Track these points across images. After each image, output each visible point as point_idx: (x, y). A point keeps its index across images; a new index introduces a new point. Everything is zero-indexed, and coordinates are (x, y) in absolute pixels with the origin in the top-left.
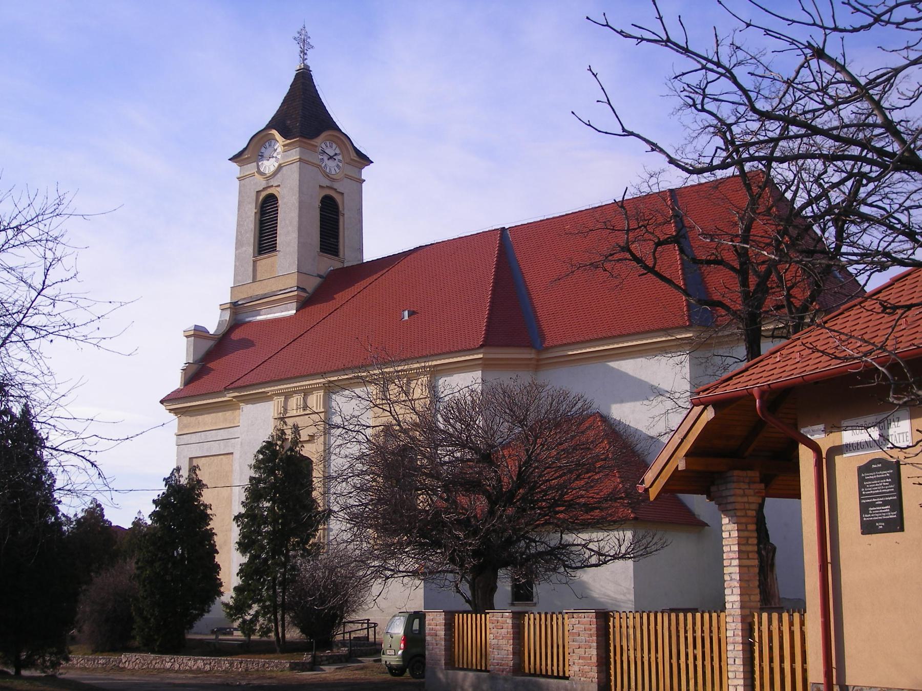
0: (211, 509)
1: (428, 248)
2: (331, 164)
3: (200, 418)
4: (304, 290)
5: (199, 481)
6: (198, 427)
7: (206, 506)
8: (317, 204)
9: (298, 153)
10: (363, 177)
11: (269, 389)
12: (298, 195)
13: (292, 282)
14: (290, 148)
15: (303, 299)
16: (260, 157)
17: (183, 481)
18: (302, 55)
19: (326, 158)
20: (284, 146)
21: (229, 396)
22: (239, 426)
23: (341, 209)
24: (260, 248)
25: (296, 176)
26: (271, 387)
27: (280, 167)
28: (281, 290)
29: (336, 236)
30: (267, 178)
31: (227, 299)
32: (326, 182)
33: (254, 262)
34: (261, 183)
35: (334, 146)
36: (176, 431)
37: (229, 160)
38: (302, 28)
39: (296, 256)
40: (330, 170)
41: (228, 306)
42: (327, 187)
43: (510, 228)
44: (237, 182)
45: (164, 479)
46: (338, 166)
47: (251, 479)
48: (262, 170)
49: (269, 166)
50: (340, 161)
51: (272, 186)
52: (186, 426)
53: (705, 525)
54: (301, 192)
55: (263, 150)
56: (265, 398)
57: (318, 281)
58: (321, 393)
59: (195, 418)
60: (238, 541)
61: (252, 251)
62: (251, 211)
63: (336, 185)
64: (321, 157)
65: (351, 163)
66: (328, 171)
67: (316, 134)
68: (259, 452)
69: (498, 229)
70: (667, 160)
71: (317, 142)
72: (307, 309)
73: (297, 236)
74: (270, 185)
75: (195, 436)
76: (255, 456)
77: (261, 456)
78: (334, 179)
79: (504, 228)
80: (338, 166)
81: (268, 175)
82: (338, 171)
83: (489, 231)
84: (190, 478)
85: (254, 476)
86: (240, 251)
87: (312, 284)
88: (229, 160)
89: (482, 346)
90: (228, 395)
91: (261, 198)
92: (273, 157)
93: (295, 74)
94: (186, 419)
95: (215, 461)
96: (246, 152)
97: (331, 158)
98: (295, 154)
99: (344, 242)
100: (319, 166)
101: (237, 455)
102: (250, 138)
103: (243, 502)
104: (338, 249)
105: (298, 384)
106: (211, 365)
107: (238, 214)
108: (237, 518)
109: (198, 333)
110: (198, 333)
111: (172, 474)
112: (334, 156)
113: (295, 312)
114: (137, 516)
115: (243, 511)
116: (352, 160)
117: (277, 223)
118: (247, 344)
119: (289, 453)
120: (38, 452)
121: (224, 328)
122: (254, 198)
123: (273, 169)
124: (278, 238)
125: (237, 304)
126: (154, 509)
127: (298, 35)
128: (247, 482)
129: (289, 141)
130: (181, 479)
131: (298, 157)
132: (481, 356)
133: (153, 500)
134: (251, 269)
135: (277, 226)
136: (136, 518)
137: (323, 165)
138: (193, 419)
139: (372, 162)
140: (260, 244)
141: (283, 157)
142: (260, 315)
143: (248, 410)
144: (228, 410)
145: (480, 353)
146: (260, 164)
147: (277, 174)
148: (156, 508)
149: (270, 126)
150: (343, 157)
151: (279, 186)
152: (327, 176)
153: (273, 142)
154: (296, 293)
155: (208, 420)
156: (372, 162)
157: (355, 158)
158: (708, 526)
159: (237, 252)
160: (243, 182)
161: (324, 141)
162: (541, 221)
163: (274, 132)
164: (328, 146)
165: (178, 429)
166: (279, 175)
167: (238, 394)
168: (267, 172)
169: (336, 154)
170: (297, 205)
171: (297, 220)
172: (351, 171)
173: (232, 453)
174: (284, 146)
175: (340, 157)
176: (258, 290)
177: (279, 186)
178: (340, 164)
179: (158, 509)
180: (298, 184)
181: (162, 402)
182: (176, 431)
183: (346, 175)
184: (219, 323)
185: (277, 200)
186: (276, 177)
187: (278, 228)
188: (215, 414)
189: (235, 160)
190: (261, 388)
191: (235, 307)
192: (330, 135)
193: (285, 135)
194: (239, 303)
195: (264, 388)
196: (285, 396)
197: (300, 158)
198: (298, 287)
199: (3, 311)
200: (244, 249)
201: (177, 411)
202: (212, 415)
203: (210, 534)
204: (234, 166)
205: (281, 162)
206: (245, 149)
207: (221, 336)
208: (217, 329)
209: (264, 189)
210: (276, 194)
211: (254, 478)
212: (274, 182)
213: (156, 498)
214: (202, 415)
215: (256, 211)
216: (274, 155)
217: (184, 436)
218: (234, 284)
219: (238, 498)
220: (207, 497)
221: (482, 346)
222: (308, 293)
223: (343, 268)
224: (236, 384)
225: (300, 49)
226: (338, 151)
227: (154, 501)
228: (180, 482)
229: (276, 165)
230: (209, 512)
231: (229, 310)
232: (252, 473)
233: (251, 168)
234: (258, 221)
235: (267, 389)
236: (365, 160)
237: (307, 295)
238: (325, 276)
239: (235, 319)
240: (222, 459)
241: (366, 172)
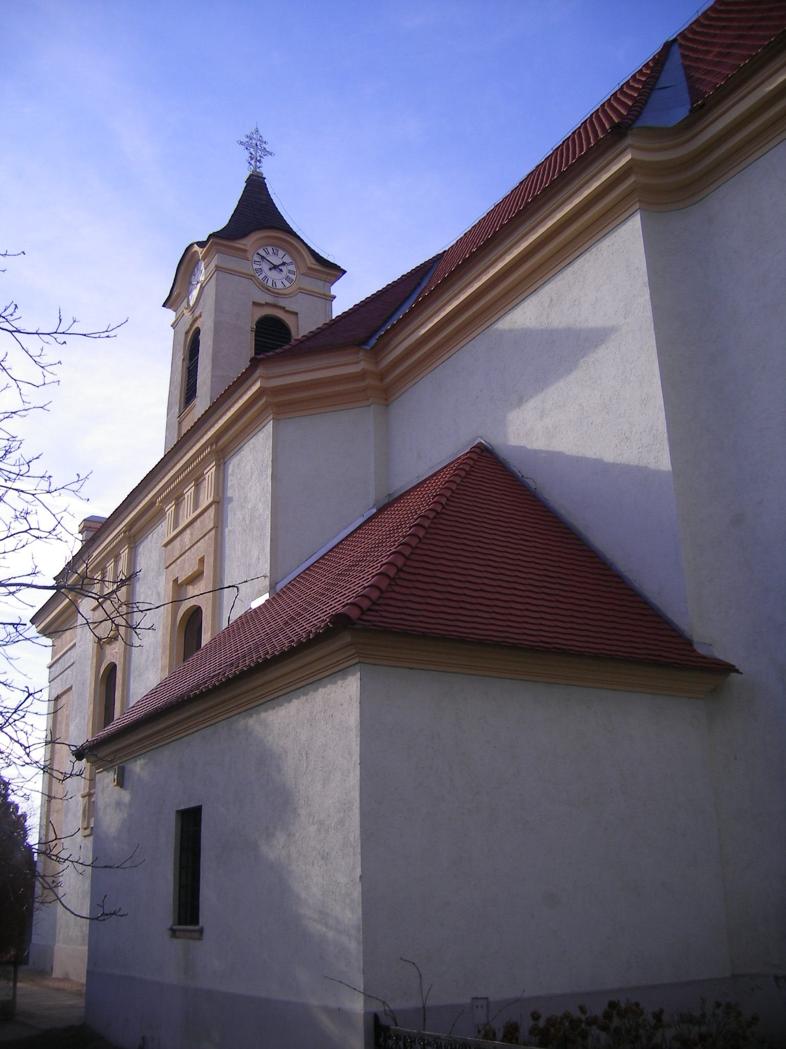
18: (253, 162)
19: (265, 267)
32: (268, 299)
38: (253, 131)
46: (287, 278)
53: (729, 669)
63: (282, 302)
65: (310, 273)
70: (286, 308)
71: (245, 245)
82: (287, 284)
97: (274, 267)
100: (251, 277)
102: (185, 249)
116: (310, 269)
120: (609, 131)
150: (297, 267)
158: (737, 671)
169: (284, 264)
172: (309, 283)
178: (293, 277)
199: (10, 400)
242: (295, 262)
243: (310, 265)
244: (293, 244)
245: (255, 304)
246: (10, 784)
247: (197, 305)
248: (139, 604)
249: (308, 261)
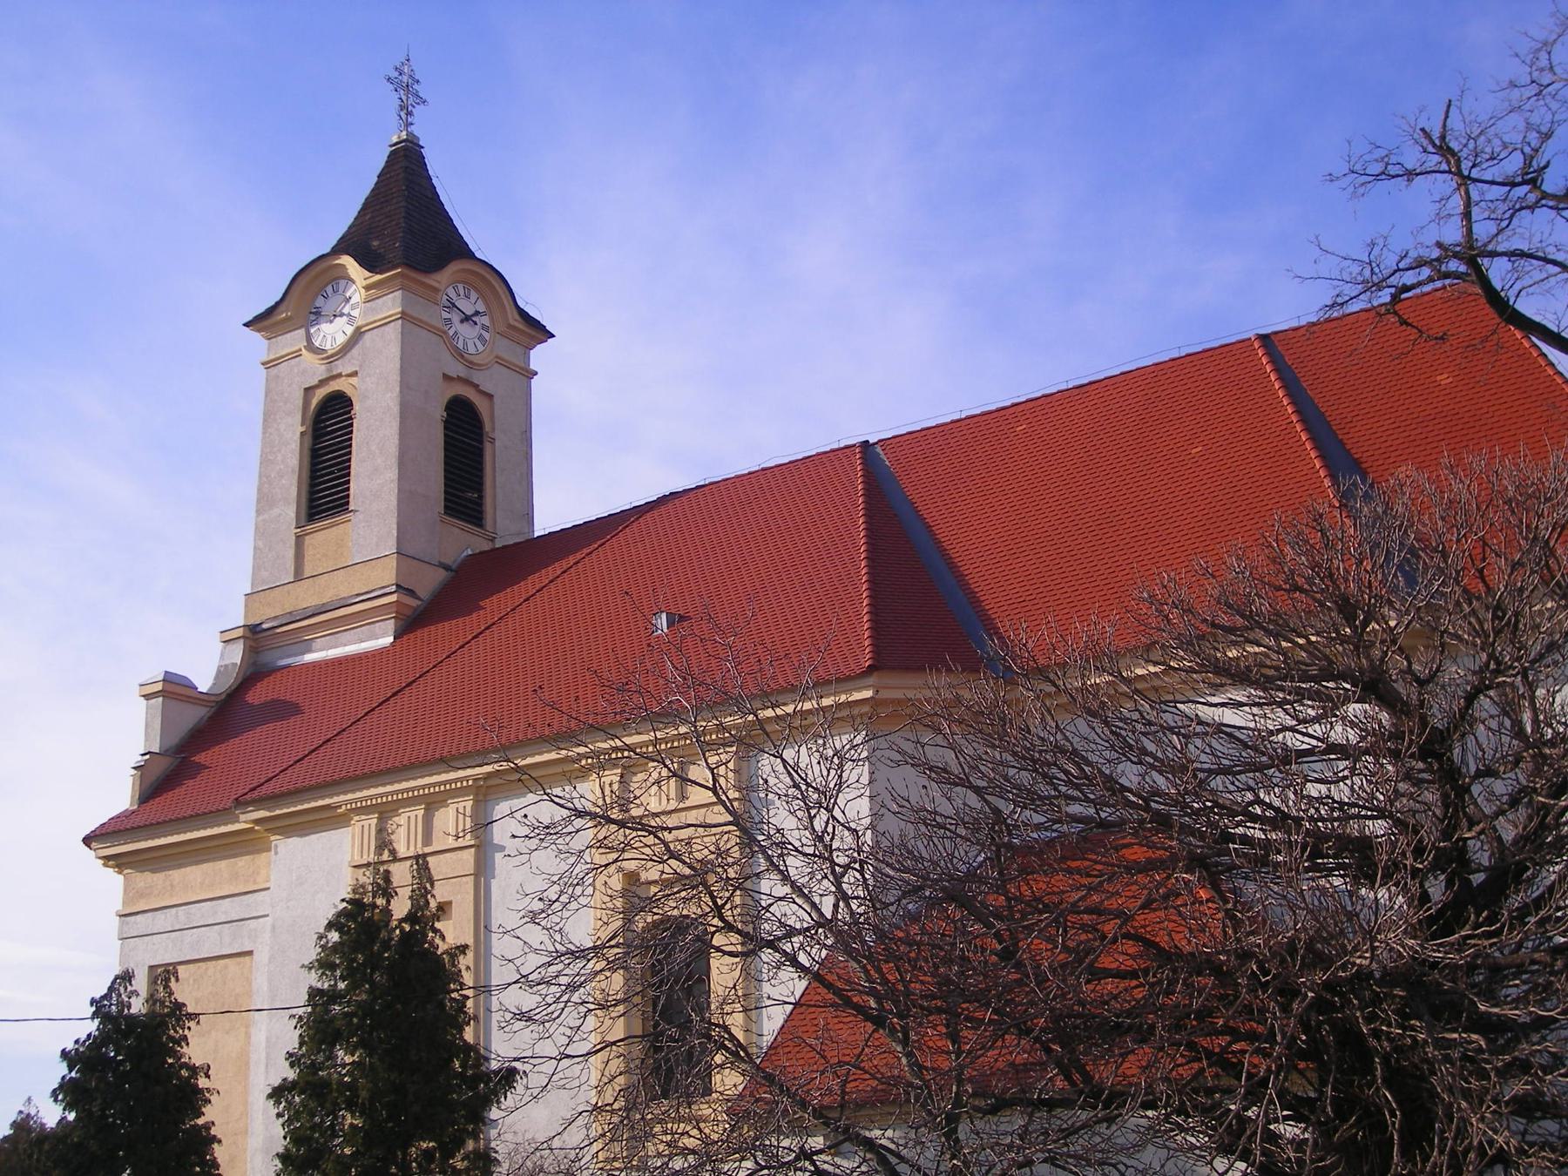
0: (208, 1076)
1: (691, 494)
2: (467, 331)
3: (176, 875)
4: (411, 593)
5: (179, 1006)
6: (171, 896)
7: (194, 1070)
8: (439, 413)
9: (399, 301)
10: (533, 366)
11: (342, 798)
12: (398, 389)
13: (386, 575)
14: (380, 293)
15: (409, 612)
16: (313, 317)
17: (138, 1006)
18: (403, 114)
19: (456, 318)
20: (367, 288)
21: (245, 820)
22: (268, 889)
23: (487, 427)
24: (311, 507)
25: (394, 351)
26: (345, 793)
27: (358, 334)
28: (358, 595)
29: (477, 484)
30: (328, 358)
31: (236, 617)
32: (457, 369)
33: (299, 539)
34: (312, 368)
35: (474, 296)
36: (119, 907)
37: (246, 325)
39: (395, 520)
40: (465, 343)
41: (240, 632)
42: (459, 379)
43: (880, 441)
44: (262, 370)
45: (93, 1002)
46: (480, 337)
47: (314, 993)
48: (317, 344)
49: (332, 333)
50: (484, 327)
51: (340, 375)
52: (141, 895)
54: (405, 385)
55: (320, 302)
56: (330, 819)
57: (441, 575)
58: (467, 804)
59: (161, 875)
60: (281, 1150)
61: (293, 515)
62: (292, 430)
63: (477, 378)
64: (446, 315)
65: (509, 333)
66: (460, 345)
67: (437, 265)
68: (330, 926)
69: (854, 445)
71: (439, 282)
72: (419, 632)
73: (396, 477)
74: (334, 373)
75: (163, 917)
76: (321, 937)
77: (334, 936)
78: (471, 363)
79: (868, 441)
80: (480, 337)
81: (330, 353)
82: (481, 348)
83: (833, 451)
84: (152, 999)
85: (319, 985)
86: (266, 516)
87: (429, 582)
88: (246, 325)
89: (871, 670)
90: (243, 817)
91: (315, 402)
92: (342, 315)
93: (388, 154)
94: (144, 879)
95: (210, 972)
96: (282, 307)
97: (466, 319)
98: (392, 304)
99: (494, 496)
100: (441, 334)
101: (261, 956)
102: (320, 254)
103: (290, 1055)
104: (481, 512)
105: (412, 784)
106: (200, 758)
107: (264, 438)
108: (277, 1094)
109: (171, 688)
110: (173, 689)
111: (111, 989)
112: (473, 315)
113: (391, 639)
114: (23, 1109)
115: (291, 1075)
117: (350, 453)
118: (282, 710)
119: (407, 928)
121: (230, 681)
122: (300, 402)
123: (341, 339)
124: (352, 484)
125: (258, 629)
126: (66, 1071)
127: (396, 74)
128: (303, 997)
129: (378, 277)
130: (133, 1000)
131: (400, 309)
132: (868, 694)
133: (63, 1051)
134: (291, 553)
135: (349, 460)
136: (21, 1112)
137: (451, 332)
138: (158, 879)
139: (553, 336)
140: (312, 486)
141: (365, 313)
142: (310, 651)
143: (290, 852)
144: (242, 855)
145: (866, 688)
146: (312, 331)
147: (351, 349)
148: (70, 1071)
149: (342, 247)
150: (492, 320)
151: (355, 374)
152: (460, 355)
153: (342, 283)
154: (394, 598)
155: (193, 878)
156: (553, 336)
157: (517, 324)
159: (261, 518)
160: (274, 371)
161: (454, 283)
162: (953, 422)
163: (348, 262)
164: (462, 292)
165: (124, 903)
166: (355, 351)
167: (268, 814)
168: (328, 347)
169: (477, 313)
170: (396, 409)
171: (397, 442)
172: (506, 349)
173: (250, 953)
174: (367, 288)
175: (485, 320)
176: (307, 596)
177: (355, 374)
178: (486, 335)
179: (73, 1074)
180: (398, 366)
181: (87, 841)
182: (119, 907)
183: (497, 357)
184: (219, 671)
185: (352, 405)
186: (349, 356)
187: (353, 464)
188: (211, 864)
189: (260, 325)
190: (322, 797)
191: (255, 636)
192: (469, 270)
193: (370, 262)
194: (265, 626)
195: (331, 796)
196: (381, 813)
197: (403, 313)
198: (398, 586)
200: (276, 511)
201: (124, 860)
202: (205, 866)
203: (204, 1140)
204: (256, 338)
205: (360, 324)
206: (278, 304)
207: (223, 697)
208: (214, 684)
209: (322, 383)
210: (349, 392)
211: (320, 992)
212: (344, 367)
213: (70, 1046)
214: (180, 866)
215: (303, 429)
216: (346, 311)
217: (139, 917)
218: (252, 589)
219: (263, 1055)
220: (196, 1049)
221: (871, 670)
222: (418, 598)
223: (494, 550)
224: (264, 790)
225: (399, 102)
226: (481, 307)
227: (65, 1054)
228: (129, 1007)
229: (350, 330)
230: (202, 1082)
231: (242, 641)
232: (313, 979)
233: (294, 340)
234: (307, 452)
235: (336, 799)
236: (538, 332)
237: (420, 603)
238: (454, 567)
239: (254, 664)
240: (226, 967)
241: (539, 357)
242: (489, 312)
243: (512, 322)
244: (494, 287)
245: (446, 377)
246: (1459, 185)
247: (345, 355)
248: (1542, 277)
249: (510, 316)
